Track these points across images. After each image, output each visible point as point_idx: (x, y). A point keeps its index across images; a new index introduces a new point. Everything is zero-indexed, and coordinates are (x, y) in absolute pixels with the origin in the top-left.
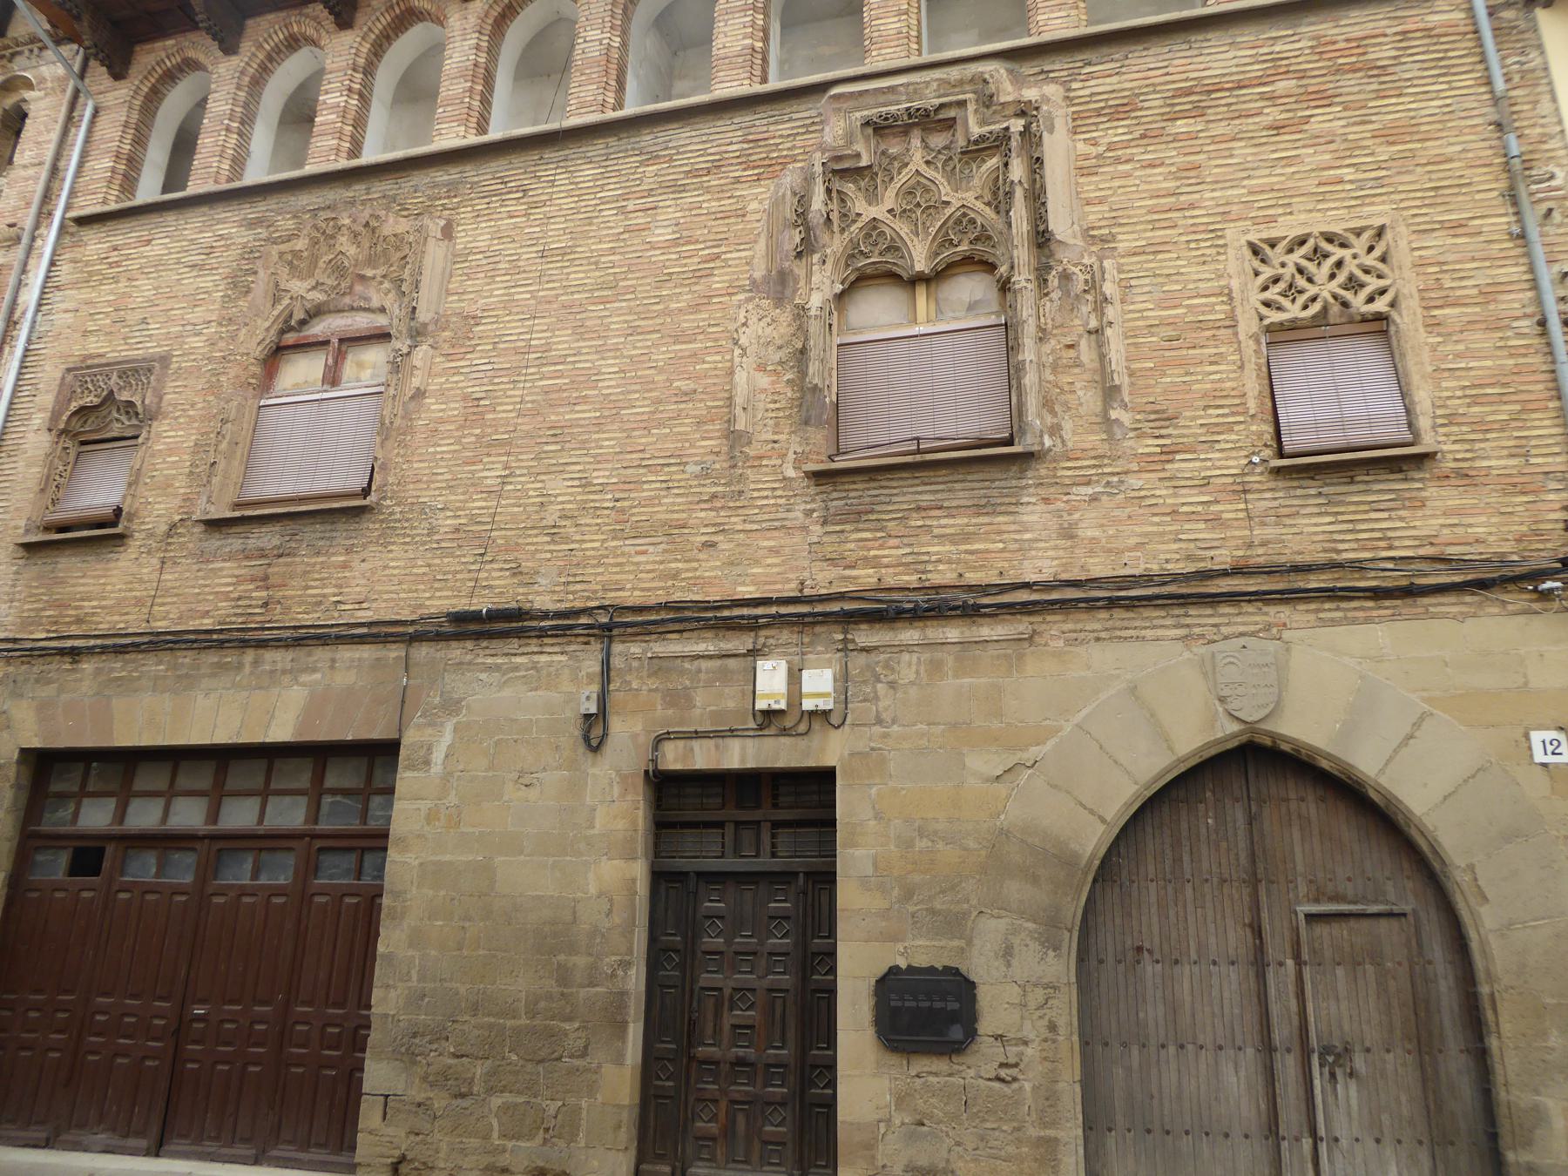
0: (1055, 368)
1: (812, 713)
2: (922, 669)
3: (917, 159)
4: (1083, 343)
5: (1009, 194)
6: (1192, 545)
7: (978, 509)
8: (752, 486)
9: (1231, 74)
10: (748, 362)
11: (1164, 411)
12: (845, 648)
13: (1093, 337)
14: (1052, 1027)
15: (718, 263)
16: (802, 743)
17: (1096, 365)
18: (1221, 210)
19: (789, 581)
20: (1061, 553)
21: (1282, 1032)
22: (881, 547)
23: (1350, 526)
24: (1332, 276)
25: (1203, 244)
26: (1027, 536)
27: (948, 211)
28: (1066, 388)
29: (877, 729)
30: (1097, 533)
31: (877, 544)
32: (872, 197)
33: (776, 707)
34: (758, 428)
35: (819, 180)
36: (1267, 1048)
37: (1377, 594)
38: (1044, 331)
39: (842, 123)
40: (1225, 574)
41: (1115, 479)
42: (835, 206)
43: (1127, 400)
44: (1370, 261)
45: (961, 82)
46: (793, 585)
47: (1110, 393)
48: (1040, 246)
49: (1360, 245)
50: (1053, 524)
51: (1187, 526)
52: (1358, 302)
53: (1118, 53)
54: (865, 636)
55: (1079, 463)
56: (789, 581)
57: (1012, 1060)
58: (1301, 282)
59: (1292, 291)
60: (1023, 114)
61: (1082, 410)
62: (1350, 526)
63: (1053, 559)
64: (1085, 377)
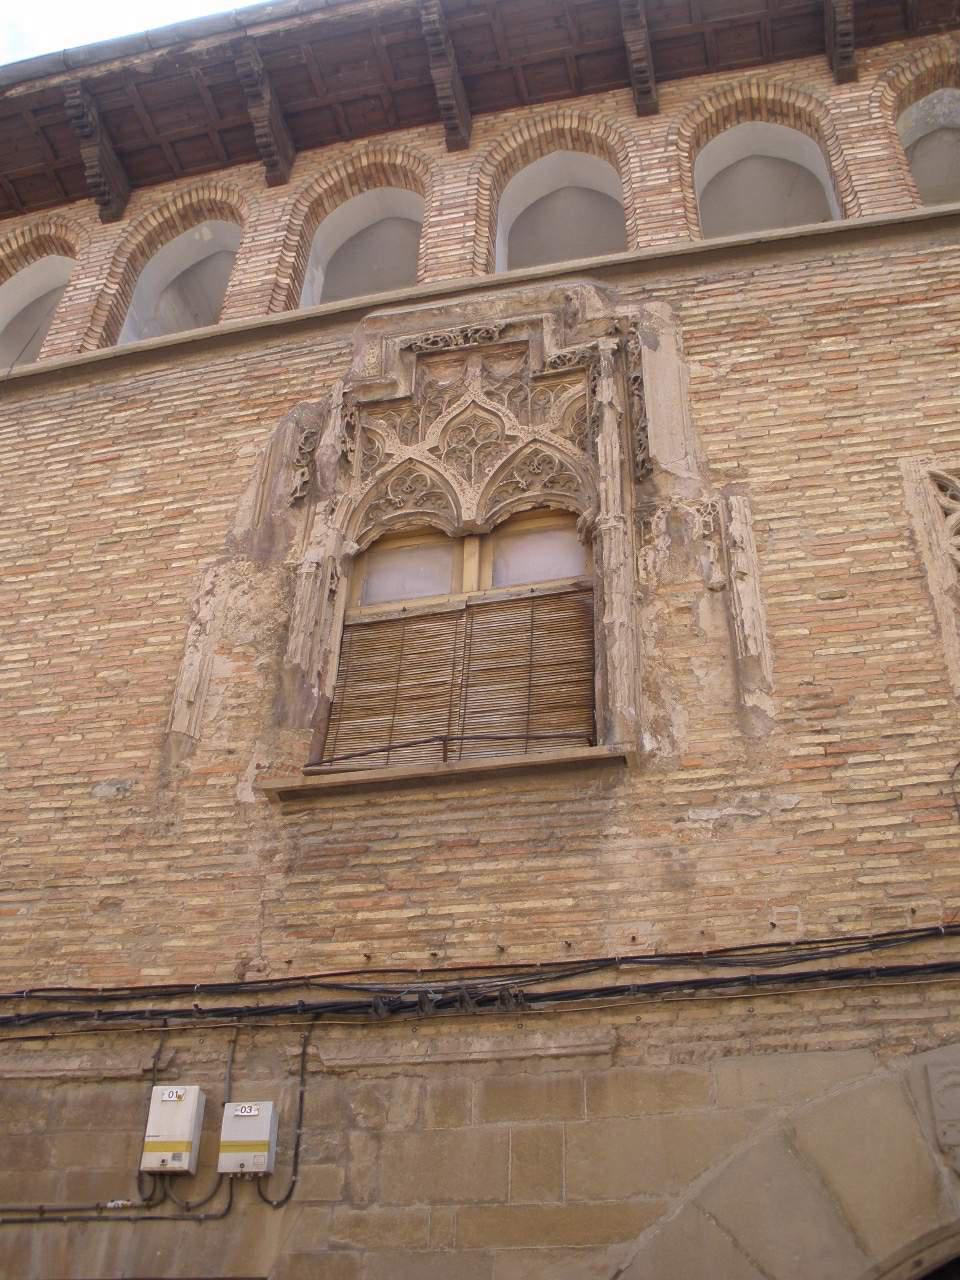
0: (661, 640)
1: (236, 1179)
2: (428, 1106)
4: (704, 605)
5: (597, 421)
6: (880, 894)
8: (188, 816)
9: (887, 290)
11: (827, 695)
13: (719, 595)
15: (188, 519)
16: (213, 1231)
17: (722, 633)
18: (889, 436)
19: (225, 958)
20: (669, 912)
22: (376, 907)
25: (868, 477)
26: (613, 886)
27: (513, 448)
28: (679, 666)
29: (345, 1211)
30: (727, 879)
31: (369, 902)
33: (173, 1165)
34: (207, 731)
35: (336, 413)
38: (645, 590)
39: (376, 350)
40: (934, 934)
41: (755, 795)
42: (357, 446)
43: (769, 678)
45: (536, 301)
46: (230, 966)
47: (741, 668)
48: (638, 481)
50: (657, 866)
51: (870, 864)
53: (741, 268)
54: (336, 1047)
55: (700, 774)
56: (225, 958)
60: (617, 332)
61: (703, 697)
63: (654, 922)
64: (706, 650)
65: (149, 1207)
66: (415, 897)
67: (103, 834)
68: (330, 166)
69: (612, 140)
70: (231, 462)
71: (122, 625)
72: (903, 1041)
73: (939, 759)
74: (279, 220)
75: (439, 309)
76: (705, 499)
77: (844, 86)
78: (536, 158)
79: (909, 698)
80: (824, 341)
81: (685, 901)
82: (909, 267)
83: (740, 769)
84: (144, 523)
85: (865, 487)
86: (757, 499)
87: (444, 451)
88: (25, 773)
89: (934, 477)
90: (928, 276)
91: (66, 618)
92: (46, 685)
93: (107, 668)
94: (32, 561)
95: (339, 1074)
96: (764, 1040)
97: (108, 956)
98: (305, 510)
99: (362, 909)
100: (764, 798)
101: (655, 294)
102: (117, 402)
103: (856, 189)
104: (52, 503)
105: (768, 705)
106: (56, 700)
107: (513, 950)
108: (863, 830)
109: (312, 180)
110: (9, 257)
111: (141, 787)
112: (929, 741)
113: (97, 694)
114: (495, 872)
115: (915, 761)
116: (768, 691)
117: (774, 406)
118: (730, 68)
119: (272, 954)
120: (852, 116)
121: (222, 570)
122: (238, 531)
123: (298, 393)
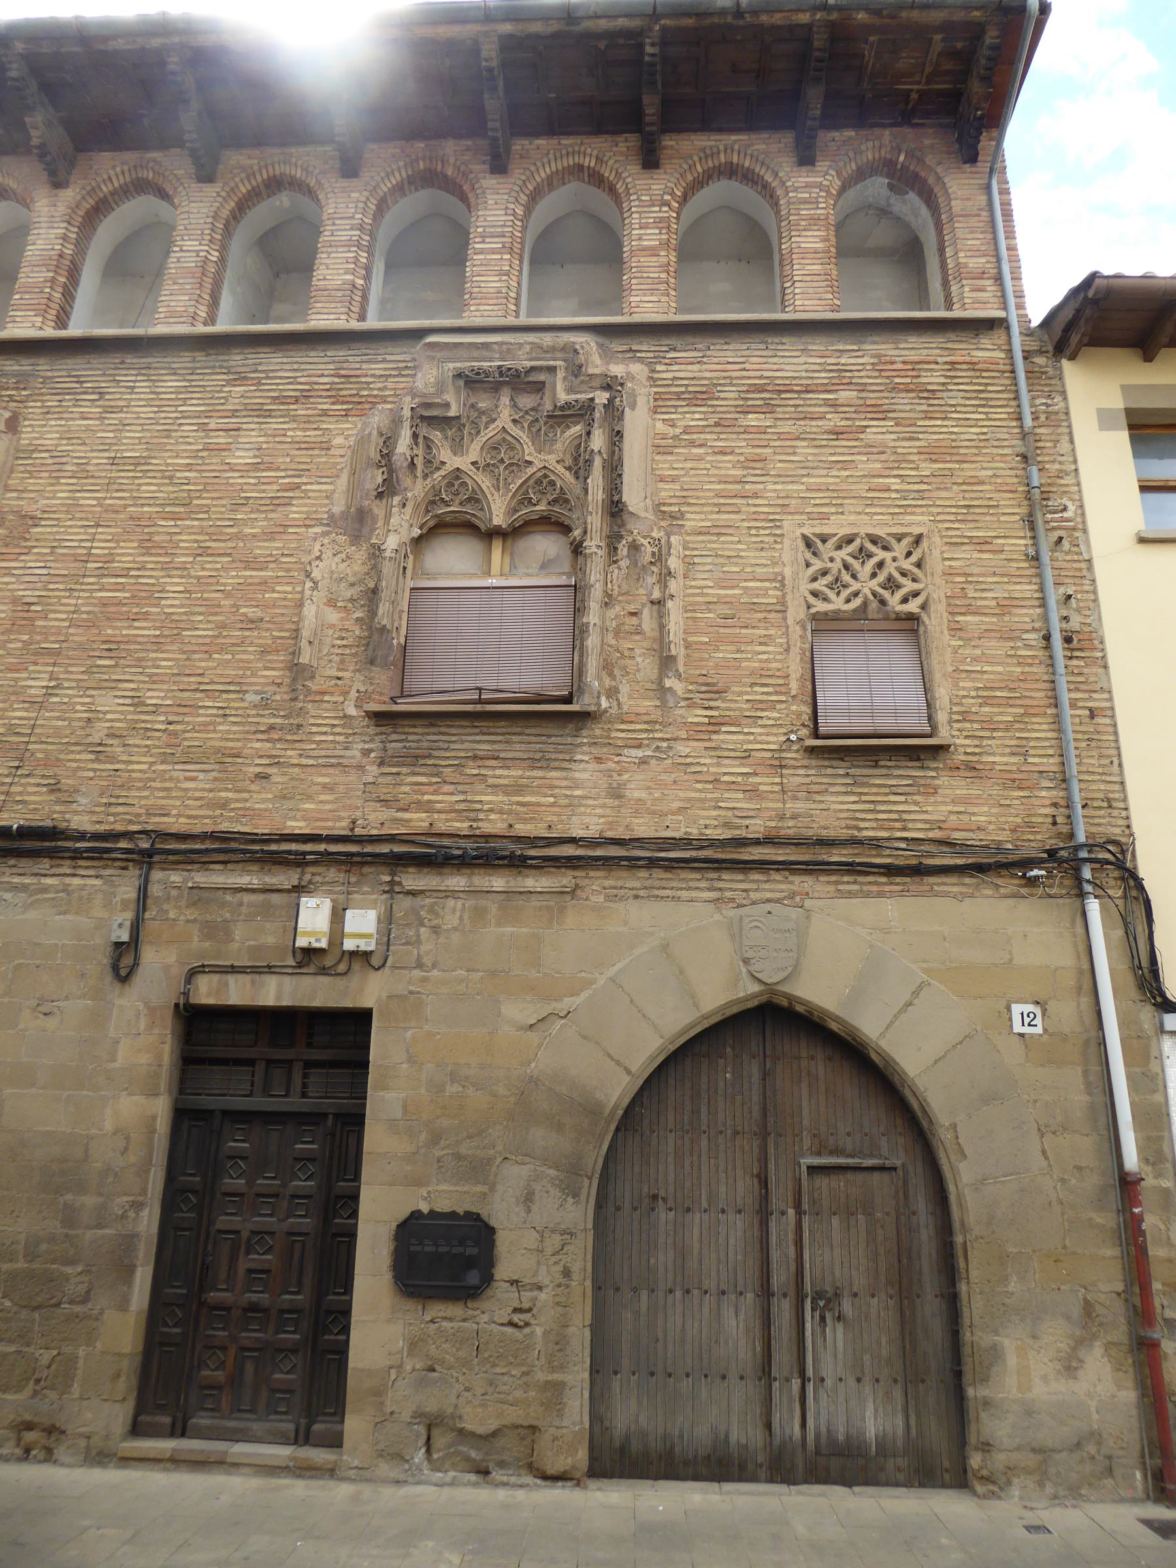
0: (617, 633)
1: (353, 954)
2: (466, 917)
3: (505, 416)
5: (589, 462)
6: (730, 813)
7: (534, 763)
8: (312, 721)
9: (801, 378)
10: (320, 596)
11: (714, 685)
12: (392, 890)
13: (656, 607)
14: (567, 1273)
15: (297, 493)
16: (340, 983)
17: (656, 634)
18: (780, 502)
19: (341, 819)
20: (608, 811)
21: (780, 1278)
23: (872, 807)
24: (874, 575)
25: (762, 532)
26: (578, 793)
27: (530, 471)
28: (626, 653)
29: (417, 973)
30: (643, 795)
31: (431, 789)
32: (458, 447)
36: (766, 1292)
37: (891, 871)
38: (610, 596)
39: (434, 372)
40: (757, 842)
41: (665, 744)
42: (420, 451)
43: (681, 669)
44: (907, 565)
45: (553, 349)
47: (666, 662)
49: (900, 549)
50: (603, 782)
52: (894, 601)
54: (411, 880)
55: (632, 727)
57: (526, 1305)
58: (846, 577)
59: (837, 585)
61: (639, 676)
62: (872, 807)
65: (300, 967)
66: (460, 788)
67: (253, 729)
68: (394, 167)
69: (620, 188)
70: (328, 449)
71: (254, 573)
72: (732, 900)
73: (775, 735)
74: (353, 218)
75: (482, 344)
76: (655, 534)
77: (804, 169)
78: (558, 187)
79: (763, 693)
80: (750, 416)
81: (619, 806)
82: (819, 360)
83: (657, 727)
84: (264, 491)
85: (759, 539)
86: (688, 538)
87: (482, 464)
88: (192, 679)
89: (804, 537)
90: (831, 371)
91: (210, 562)
92: (200, 614)
93: (246, 606)
94: (177, 509)
95: (413, 895)
96: (656, 892)
97: (264, 811)
98: (384, 500)
99: (427, 793)
100: (670, 748)
101: (638, 355)
102: (231, 377)
103: (796, 278)
104: (188, 461)
105: (678, 686)
106: (209, 626)
107: (517, 826)
108: (725, 774)
109: (379, 179)
110: (112, 194)
111: (278, 697)
112: (771, 722)
113: (240, 626)
114: (508, 777)
115: (761, 734)
116: (679, 676)
117: (708, 466)
118: (720, 130)
119: (371, 817)
120: (805, 203)
121: (326, 541)
122: (337, 510)
123: (376, 396)
